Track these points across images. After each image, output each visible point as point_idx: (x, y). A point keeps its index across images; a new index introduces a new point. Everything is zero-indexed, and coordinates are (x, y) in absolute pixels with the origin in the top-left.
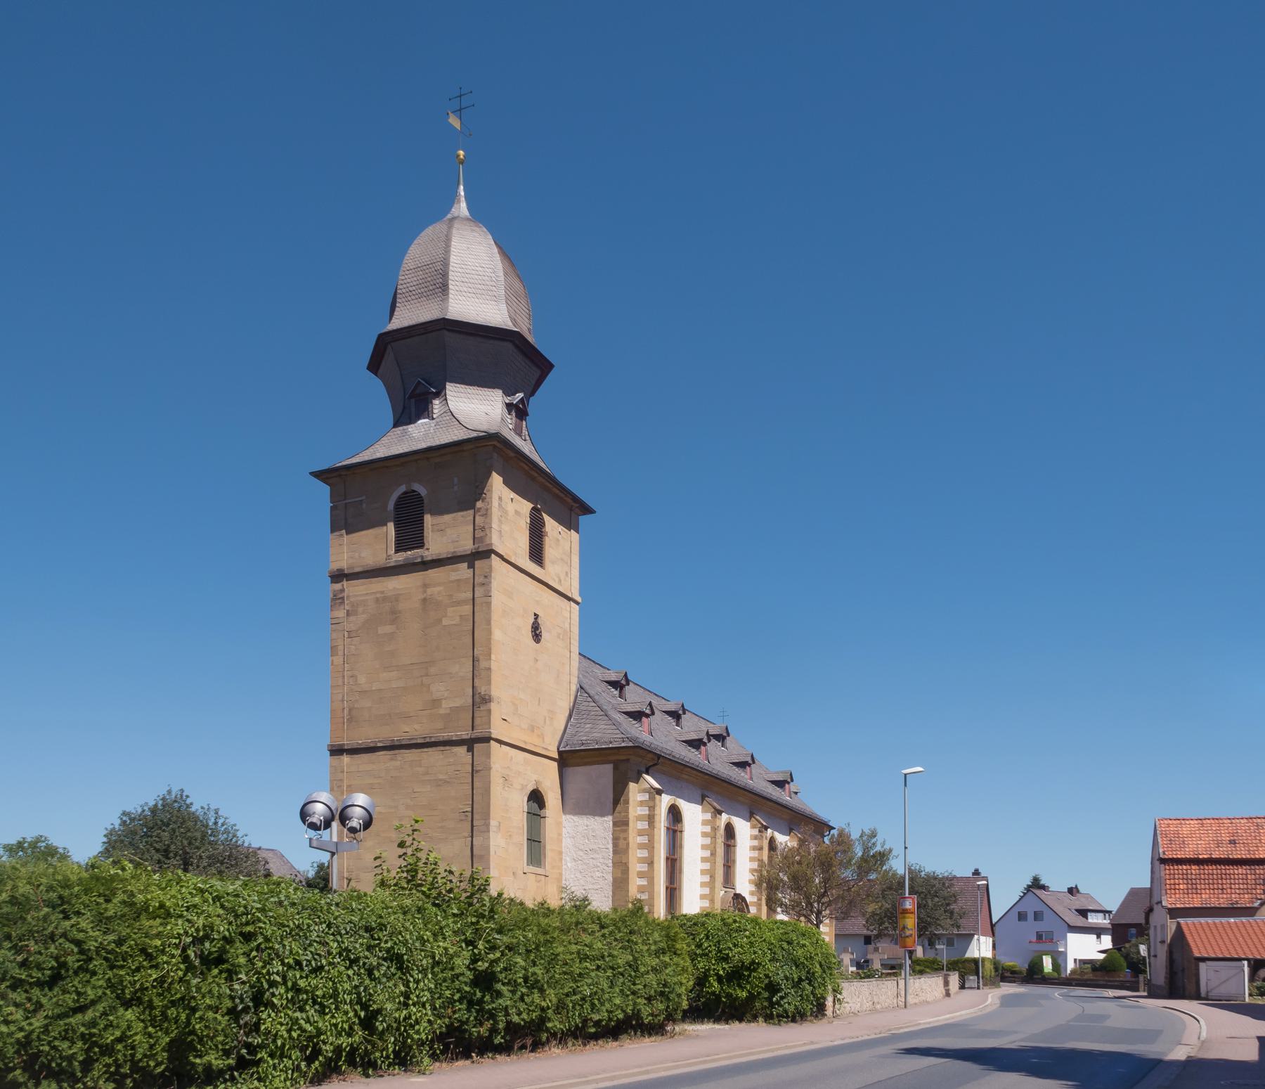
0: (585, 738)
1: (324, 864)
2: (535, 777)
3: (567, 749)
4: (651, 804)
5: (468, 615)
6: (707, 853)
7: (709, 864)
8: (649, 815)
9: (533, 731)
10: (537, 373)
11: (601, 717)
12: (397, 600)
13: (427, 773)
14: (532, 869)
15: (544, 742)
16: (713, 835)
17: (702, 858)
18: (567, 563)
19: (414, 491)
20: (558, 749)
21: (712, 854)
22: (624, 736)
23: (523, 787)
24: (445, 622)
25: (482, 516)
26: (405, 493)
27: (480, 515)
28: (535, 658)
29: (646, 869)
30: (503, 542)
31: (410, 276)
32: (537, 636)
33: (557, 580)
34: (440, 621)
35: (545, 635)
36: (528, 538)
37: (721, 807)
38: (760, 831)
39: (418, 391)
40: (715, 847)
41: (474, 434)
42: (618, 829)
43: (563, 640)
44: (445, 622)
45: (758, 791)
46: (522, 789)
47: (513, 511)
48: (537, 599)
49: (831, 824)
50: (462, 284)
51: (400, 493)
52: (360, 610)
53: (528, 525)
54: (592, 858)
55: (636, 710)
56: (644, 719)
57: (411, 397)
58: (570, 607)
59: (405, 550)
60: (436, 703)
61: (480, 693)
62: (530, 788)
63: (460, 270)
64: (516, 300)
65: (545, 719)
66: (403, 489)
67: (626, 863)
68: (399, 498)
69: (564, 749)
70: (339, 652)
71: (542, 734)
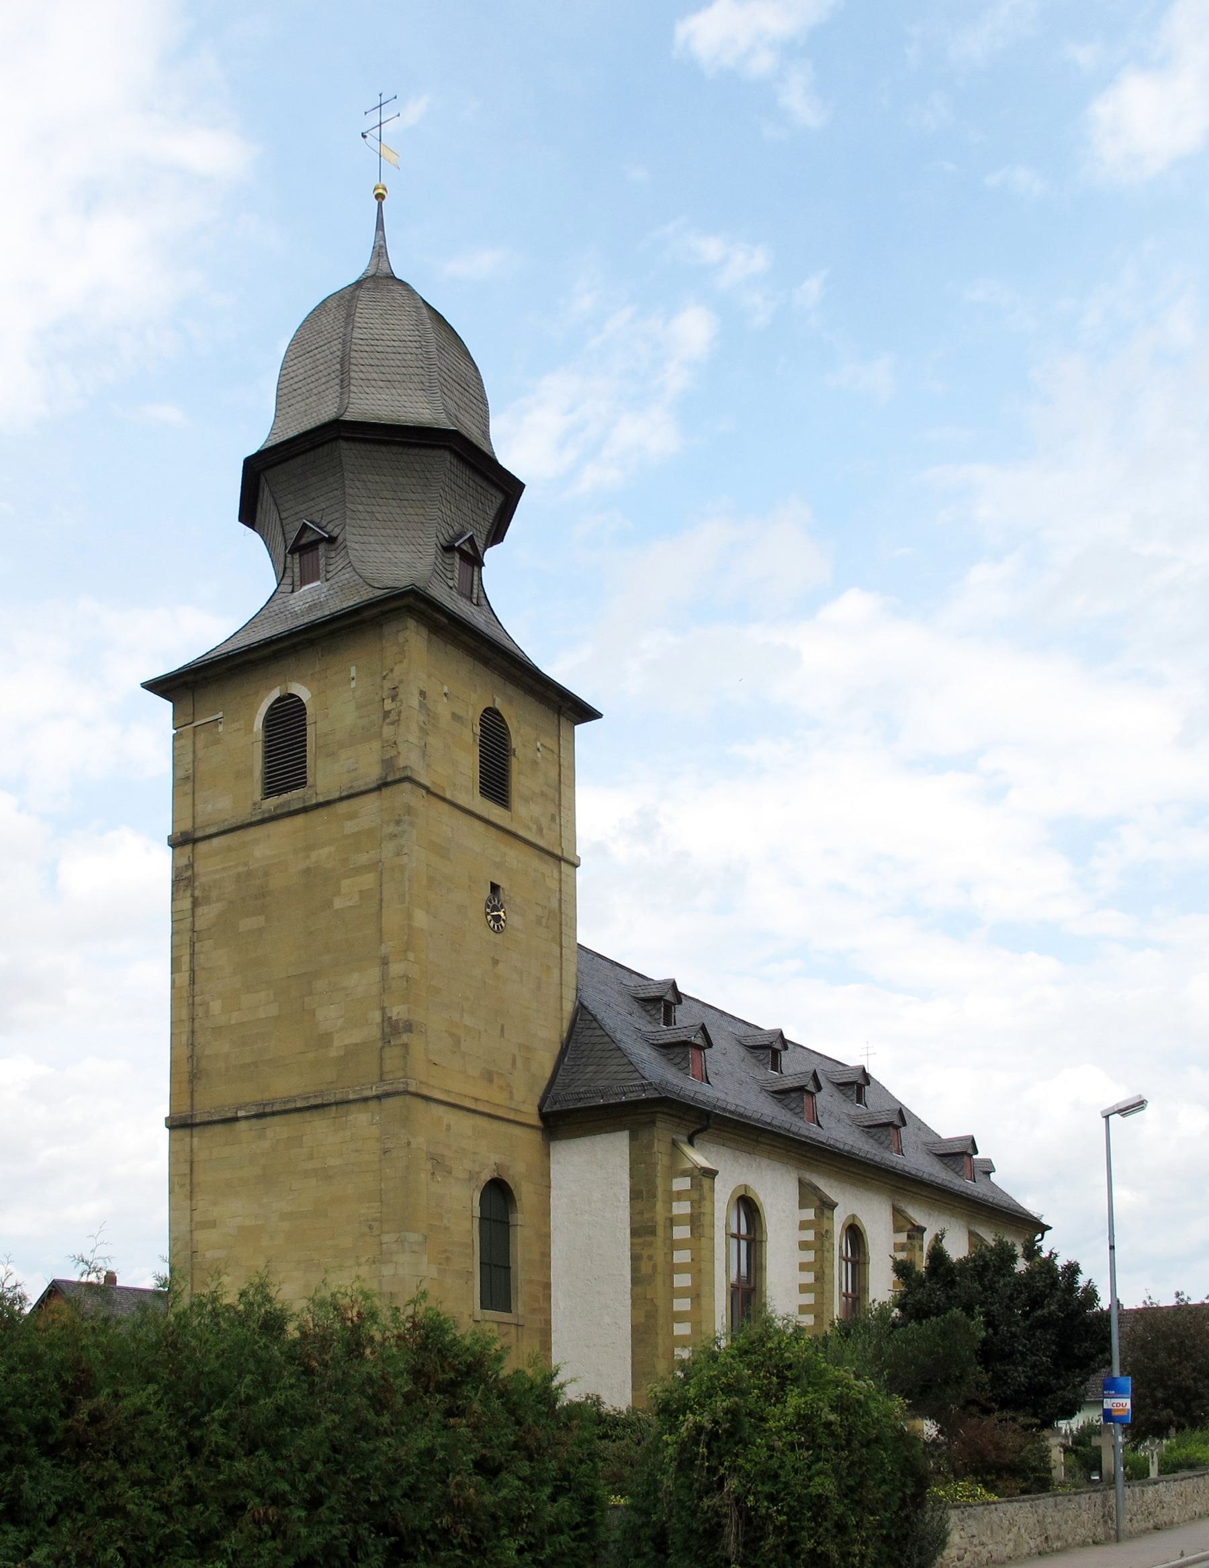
0: (583, 1089)
1: (22, 1299)
2: (495, 1158)
3: (555, 1108)
4: (695, 1196)
5: (371, 889)
6: (809, 1278)
7: (813, 1294)
8: (692, 1215)
9: (491, 1081)
10: (498, 499)
11: (611, 1053)
12: (266, 874)
13: (311, 1157)
14: (491, 1314)
15: (511, 1098)
16: (821, 1243)
17: (800, 1286)
18: (553, 800)
19: (292, 696)
20: (540, 1110)
21: (816, 1279)
22: (644, 1082)
23: (472, 1176)
24: (338, 903)
25: (392, 723)
26: (278, 700)
27: (388, 724)
28: (493, 958)
29: (689, 1308)
30: (429, 766)
31: (295, 368)
32: (1140, 1105)
33: (534, 828)
34: (328, 904)
35: (512, 918)
36: (478, 758)
37: (712, 1164)
38: (909, 1237)
39: (303, 541)
40: (822, 1267)
41: (378, 593)
42: (640, 1240)
43: (547, 927)
44: (338, 903)
45: (926, 1176)
46: (470, 1180)
47: (449, 716)
48: (498, 859)
49: (1044, 1221)
50: (370, 369)
51: (272, 700)
52: (214, 894)
53: (478, 738)
54: (598, 1292)
55: (678, 1039)
56: (692, 1053)
57: (292, 552)
58: (560, 872)
59: (280, 792)
60: (325, 1039)
61: (390, 1018)
62: (486, 1176)
63: (367, 349)
64: (458, 387)
65: (514, 1061)
66: (276, 694)
67: (652, 1300)
68: (271, 708)
69: (549, 1110)
70: (183, 967)
71: (509, 1086)
